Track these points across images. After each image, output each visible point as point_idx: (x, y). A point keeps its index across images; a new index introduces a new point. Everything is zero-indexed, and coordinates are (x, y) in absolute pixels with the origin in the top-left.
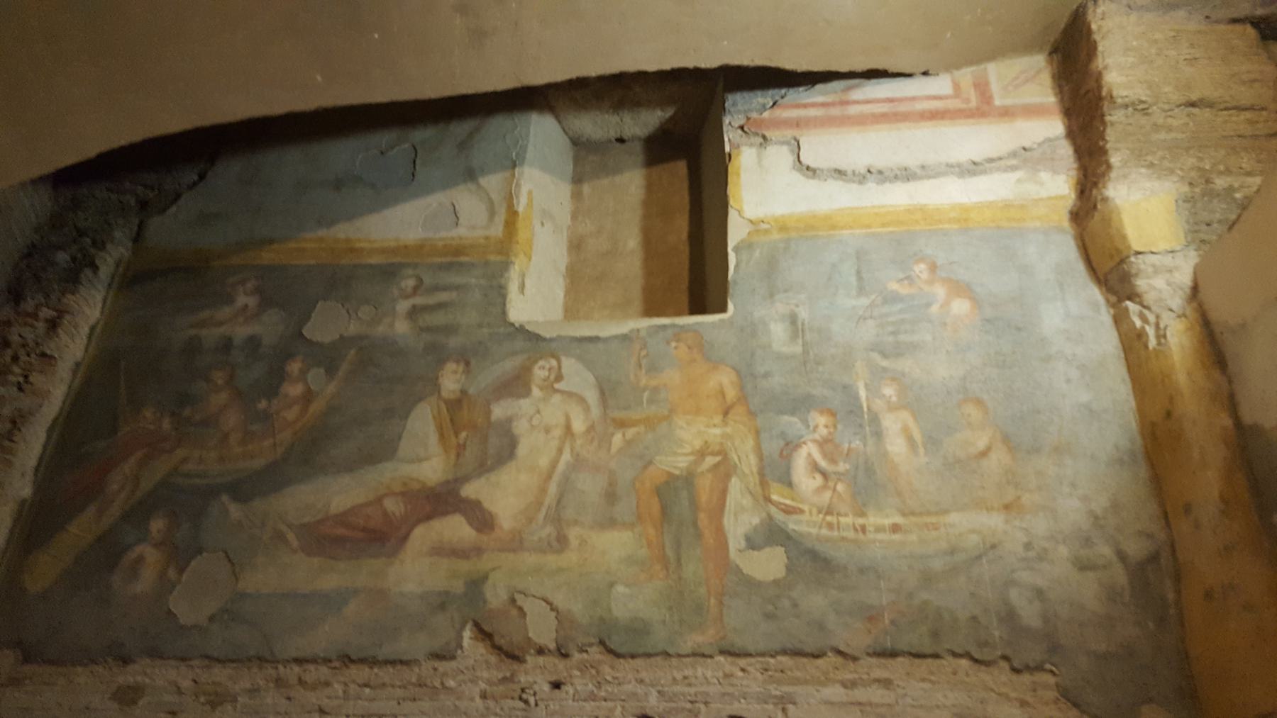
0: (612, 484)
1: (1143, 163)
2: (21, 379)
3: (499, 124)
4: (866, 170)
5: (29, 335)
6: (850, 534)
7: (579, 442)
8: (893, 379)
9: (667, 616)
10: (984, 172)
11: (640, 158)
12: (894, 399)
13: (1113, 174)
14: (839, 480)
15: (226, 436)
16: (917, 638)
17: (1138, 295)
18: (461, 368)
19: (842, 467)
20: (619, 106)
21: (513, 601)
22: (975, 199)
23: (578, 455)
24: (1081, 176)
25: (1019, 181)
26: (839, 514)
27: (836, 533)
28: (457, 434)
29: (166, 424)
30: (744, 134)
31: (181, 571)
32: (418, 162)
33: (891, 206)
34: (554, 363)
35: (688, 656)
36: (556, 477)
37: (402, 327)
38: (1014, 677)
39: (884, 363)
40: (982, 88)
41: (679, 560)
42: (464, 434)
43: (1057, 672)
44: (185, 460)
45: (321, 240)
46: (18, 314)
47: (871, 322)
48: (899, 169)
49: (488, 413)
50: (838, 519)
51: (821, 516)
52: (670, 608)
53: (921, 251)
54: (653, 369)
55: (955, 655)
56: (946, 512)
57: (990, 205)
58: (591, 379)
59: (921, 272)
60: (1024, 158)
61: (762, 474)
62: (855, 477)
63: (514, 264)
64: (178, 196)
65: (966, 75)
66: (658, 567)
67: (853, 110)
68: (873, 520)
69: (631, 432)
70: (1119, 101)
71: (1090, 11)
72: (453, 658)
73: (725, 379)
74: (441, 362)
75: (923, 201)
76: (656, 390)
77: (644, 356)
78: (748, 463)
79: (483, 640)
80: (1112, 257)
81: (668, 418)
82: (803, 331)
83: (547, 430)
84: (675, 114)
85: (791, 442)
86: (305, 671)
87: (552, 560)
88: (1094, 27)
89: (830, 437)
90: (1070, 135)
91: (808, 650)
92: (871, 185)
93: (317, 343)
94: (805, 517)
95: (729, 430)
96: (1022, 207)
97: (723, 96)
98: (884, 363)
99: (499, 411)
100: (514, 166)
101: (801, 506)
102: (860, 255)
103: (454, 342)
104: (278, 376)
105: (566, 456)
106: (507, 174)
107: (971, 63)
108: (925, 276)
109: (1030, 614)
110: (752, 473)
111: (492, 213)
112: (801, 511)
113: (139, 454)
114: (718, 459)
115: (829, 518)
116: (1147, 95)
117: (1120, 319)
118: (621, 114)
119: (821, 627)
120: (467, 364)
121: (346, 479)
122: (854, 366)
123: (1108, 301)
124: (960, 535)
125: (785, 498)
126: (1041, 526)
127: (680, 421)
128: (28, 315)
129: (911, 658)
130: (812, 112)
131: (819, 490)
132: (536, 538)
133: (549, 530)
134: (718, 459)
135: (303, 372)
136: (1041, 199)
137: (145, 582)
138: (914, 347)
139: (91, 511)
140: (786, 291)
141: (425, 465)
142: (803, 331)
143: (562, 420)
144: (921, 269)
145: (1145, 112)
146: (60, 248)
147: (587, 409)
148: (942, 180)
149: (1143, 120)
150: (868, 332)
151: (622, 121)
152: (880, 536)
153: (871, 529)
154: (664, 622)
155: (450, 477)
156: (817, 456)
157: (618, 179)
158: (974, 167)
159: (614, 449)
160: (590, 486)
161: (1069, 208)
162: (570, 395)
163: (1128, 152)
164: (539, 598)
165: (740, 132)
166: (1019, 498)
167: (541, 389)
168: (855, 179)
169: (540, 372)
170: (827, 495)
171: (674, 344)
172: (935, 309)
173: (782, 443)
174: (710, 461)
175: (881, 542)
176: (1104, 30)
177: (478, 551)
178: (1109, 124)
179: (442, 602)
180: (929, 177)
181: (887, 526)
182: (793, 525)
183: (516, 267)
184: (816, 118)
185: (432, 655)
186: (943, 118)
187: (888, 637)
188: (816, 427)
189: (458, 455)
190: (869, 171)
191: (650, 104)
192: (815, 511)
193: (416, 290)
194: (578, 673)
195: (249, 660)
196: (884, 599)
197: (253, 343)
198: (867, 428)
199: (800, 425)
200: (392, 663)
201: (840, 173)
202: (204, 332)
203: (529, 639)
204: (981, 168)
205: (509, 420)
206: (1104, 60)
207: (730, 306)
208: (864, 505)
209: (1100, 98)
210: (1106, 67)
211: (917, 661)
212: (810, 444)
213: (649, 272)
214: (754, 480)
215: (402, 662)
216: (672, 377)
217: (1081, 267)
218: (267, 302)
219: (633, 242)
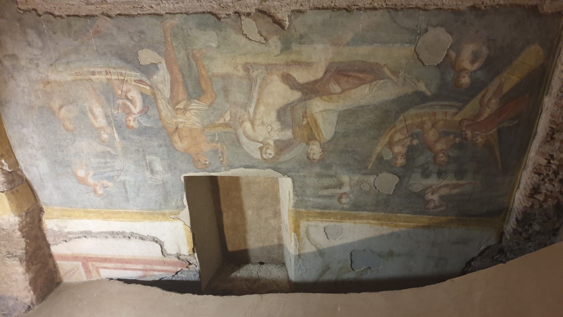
0: (226, 96)
1: (6, 231)
2: (552, 161)
3: (310, 276)
4: (131, 239)
5: (548, 186)
6: (112, 70)
7: (246, 117)
8: (104, 141)
9: (189, 32)
10: (82, 233)
11: (251, 254)
12: (102, 132)
13: (17, 227)
14: (120, 96)
15: (433, 126)
16: (78, 24)
17: (4, 173)
18: (311, 156)
19: (120, 102)
20: (257, 280)
21: (266, 39)
22: (83, 221)
23: (246, 111)
24: (41, 227)
25: (66, 228)
26: (118, 79)
27: (118, 71)
28: (308, 123)
29: (469, 133)
30: (189, 261)
31: (447, 55)
32: (350, 262)
33: (118, 221)
34: (265, 156)
35: (177, 13)
36: (255, 100)
37: (345, 178)
38: (35, 7)
39: (109, 149)
40: (88, 271)
41: (188, 59)
42: (304, 123)
43: (17, 9)
44: (455, 114)
45: (396, 226)
46: (557, 198)
47: (118, 168)
48: (116, 237)
49: (293, 133)
52: (189, 36)
53: (101, 199)
54: (216, 152)
55: (61, 17)
56: (74, 81)
57: (76, 218)
58: (245, 147)
59: (100, 190)
60: (67, 238)
61: (156, 99)
62: (114, 97)
63: (292, 207)
64: (481, 254)
66: (198, 55)
67: (140, 267)
69: (221, 121)
70: (17, 259)
71: (34, 300)
72: (293, 11)
73: (180, 145)
74: (322, 160)
76: (213, 141)
77: (220, 158)
78: (162, 104)
79: (280, 20)
80: (17, 191)
81: (204, 128)
82: (147, 166)
83: (263, 123)
84: (231, 274)
85: (144, 114)
86: (371, 4)
87: (250, 60)
88: (32, 293)
89: (127, 116)
90: (48, 246)
91: (123, 17)
92: (128, 231)
93: (390, 172)
94: (133, 78)
95: (175, 120)
96: (63, 216)
97: (201, 279)
98: (109, 149)
99: (288, 134)
100: (299, 255)
102: (127, 200)
103: (317, 169)
105: (251, 110)
106: (302, 252)
107: (93, 282)
108: (98, 188)
109: (32, 35)
110: (160, 100)
111: (307, 232)
112: (135, 81)
113: (482, 118)
114: (177, 107)
115: (123, 78)
116: (6, 260)
117: (15, 164)
118: (257, 277)
119: (119, 28)
120: (308, 157)
121: (363, 102)
122: (122, 148)
123: (22, 172)
124: (66, 70)
125: (143, 88)
126: (34, 74)
127: (198, 126)
128: (551, 197)
129: (79, 15)
130: (159, 268)
131: (129, 91)
132: (260, 71)
133: (254, 74)
134: (177, 107)
135: (395, 157)
136: (56, 218)
137: (468, 50)
138: (97, 156)
139: (505, 90)
140: (158, 185)
141: (321, 108)
142: (147, 166)
143: (256, 128)
144: (100, 192)
145: (9, 253)
146: (538, 233)
147: (244, 133)
148: (97, 231)
149: (10, 250)
150: (118, 164)
151: (258, 273)
152: (99, 70)
153: (103, 73)
154: (191, 29)
155: (308, 102)
157: (261, 245)
158: (86, 235)
159: (228, 112)
160: (237, 96)
161: (45, 214)
162: (254, 140)
163: (14, 236)
164: (253, 40)
165: (191, 262)
166: (44, 87)
167: (269, 144)
168: (136, 235)
169: (271, 152)
171: (207, 163)
172: (92, 173)
173: (148, 113)
174: (181, 106)
175: (98, 67)
176: (26, 291)
177: (288, 64)
178: (24, 249)
179: (302, 39)
180: (103, 232)
182: (138, 75)
183: (291, 205)
184: (157, 265)
185: (304, 12)
186: (102, 259)
187: (89, 23)
188: (134, 121)
189: (305, 112)
190: (129, 238)
191: (243, 280)
192: (129, 82)
193: (340, 197)
194: (230, 4)
195: (402, 9)
196: (93, 41)
197: (426, 174)
198: (112, 119)
199: (142, 121)
200: (323, 8)
201: (142, 238)
202: (455, 182)
203: (254, 21)
204: (84, 235)
205: (282, 129)
206: (26, 278)
207: (183, 179)
209: (27, 261)
210: (24, 274)
211: (77, 14)
212: (136, 112)
213: (240, 198)
214: (159, 96)
215: (319, 9)
216: (206, 147)
217: (35, 188)
219: (249, 213)
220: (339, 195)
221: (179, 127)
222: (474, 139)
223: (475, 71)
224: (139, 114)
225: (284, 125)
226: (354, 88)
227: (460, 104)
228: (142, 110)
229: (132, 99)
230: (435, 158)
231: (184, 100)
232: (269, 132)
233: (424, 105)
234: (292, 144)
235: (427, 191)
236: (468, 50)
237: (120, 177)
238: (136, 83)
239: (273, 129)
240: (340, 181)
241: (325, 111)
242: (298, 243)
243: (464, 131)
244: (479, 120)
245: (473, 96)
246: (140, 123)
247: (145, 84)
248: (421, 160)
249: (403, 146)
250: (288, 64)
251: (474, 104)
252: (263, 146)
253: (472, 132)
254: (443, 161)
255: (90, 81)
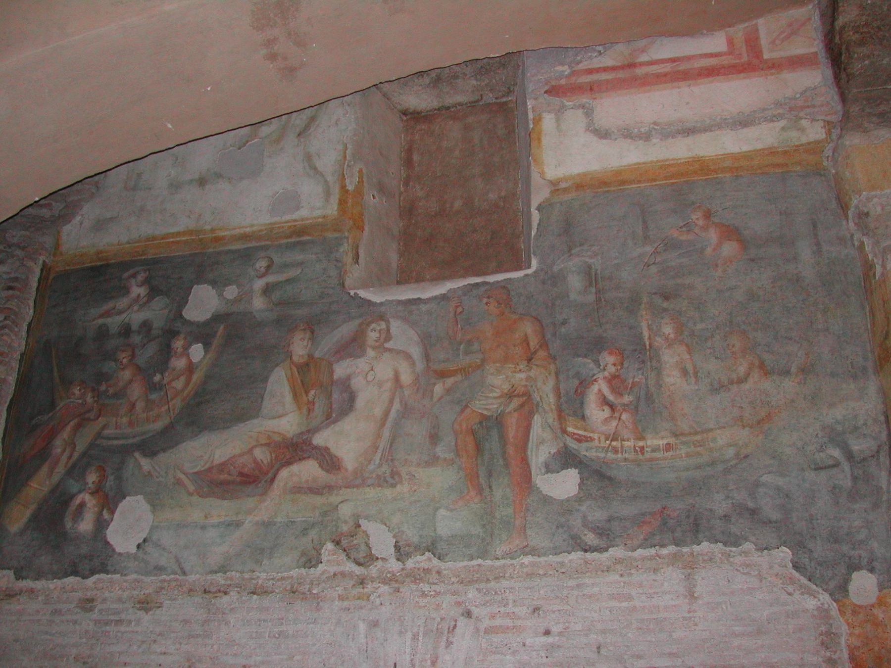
6: (631, 456)
12: (672, 336)
14: (624, 410)
15: (133, 405)
18: (308, 335)
19: (627, 399)
25: (783, 129)
27: (620, 455)
28: (307, 393)
29: (89, 399)
33: (673, 159)
39: (665, 305)
40: (752, 42)
42: (313, 392)
44: (104, 427)
49: (332, 372)
50: (621, 443)
51: (608, 442)
65: (739, 31)
67: (639, 71)
68: (652, 441)
69: (450, 381)
75: (702, 153)
83: (380, 385)
89: (617, 374)
96: (785, 153)
101: (591, 435)
104: (166, 352)
111: (328, 194)
112: (592, 439)
113: (72, 424)
115: (614, 443)
127: (490, 368)
131: (606, 421)
135: (186, 348)
139: (45, 469)
141: (284, 420)
143: (391, 374)
144: (696, 217)
147: (413, 364)
155: (304, 429)
156: (606, 391)
159: (436, 397)
162: (399, 352)
170: (614, 423)
171: (485, 300)
173: (577, 382)
181: (661, 446)
184: (608, 81)
189: (309, 410)
192: (603, 438)
197: (146, 326)
199: (592, 365)
205: (349, 378)
208: (644, 431)
218: (154, 292)
220: (271, 271)
221: (525, 363)
222: (83, 390)
223: (80, 492)
224: (595, 377)
225: (346, 385)
226: (234, 456)
227: (98, 442)
228: (588, 388)
229: (602, 405)
230: (133, 356)
231: (510, 413)
232: (372, 370)
233: (144, 437)
234: (336, 353)
235: (145, 299)
236: (86, 525)
237: (652, 252)
238: (590, 437)
239: (365, 376)
240: (267, 296)
241: (280, 417)
242: (345, 173)
243: (95, 401)
244: (76, 421)
245: (84, 454)
246: (597, 363)
247: (575, 437)
248: (152, 349)
249: (174, 370)
250: (330, 488)
251: (81, 446)
252: (385, 344)
253: (85, 401)
254: (123, 351)
255: (678, 433)
